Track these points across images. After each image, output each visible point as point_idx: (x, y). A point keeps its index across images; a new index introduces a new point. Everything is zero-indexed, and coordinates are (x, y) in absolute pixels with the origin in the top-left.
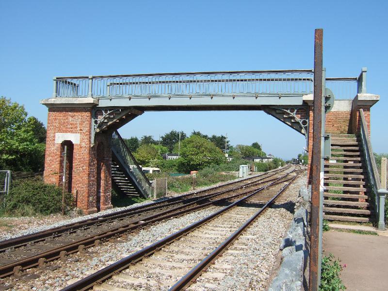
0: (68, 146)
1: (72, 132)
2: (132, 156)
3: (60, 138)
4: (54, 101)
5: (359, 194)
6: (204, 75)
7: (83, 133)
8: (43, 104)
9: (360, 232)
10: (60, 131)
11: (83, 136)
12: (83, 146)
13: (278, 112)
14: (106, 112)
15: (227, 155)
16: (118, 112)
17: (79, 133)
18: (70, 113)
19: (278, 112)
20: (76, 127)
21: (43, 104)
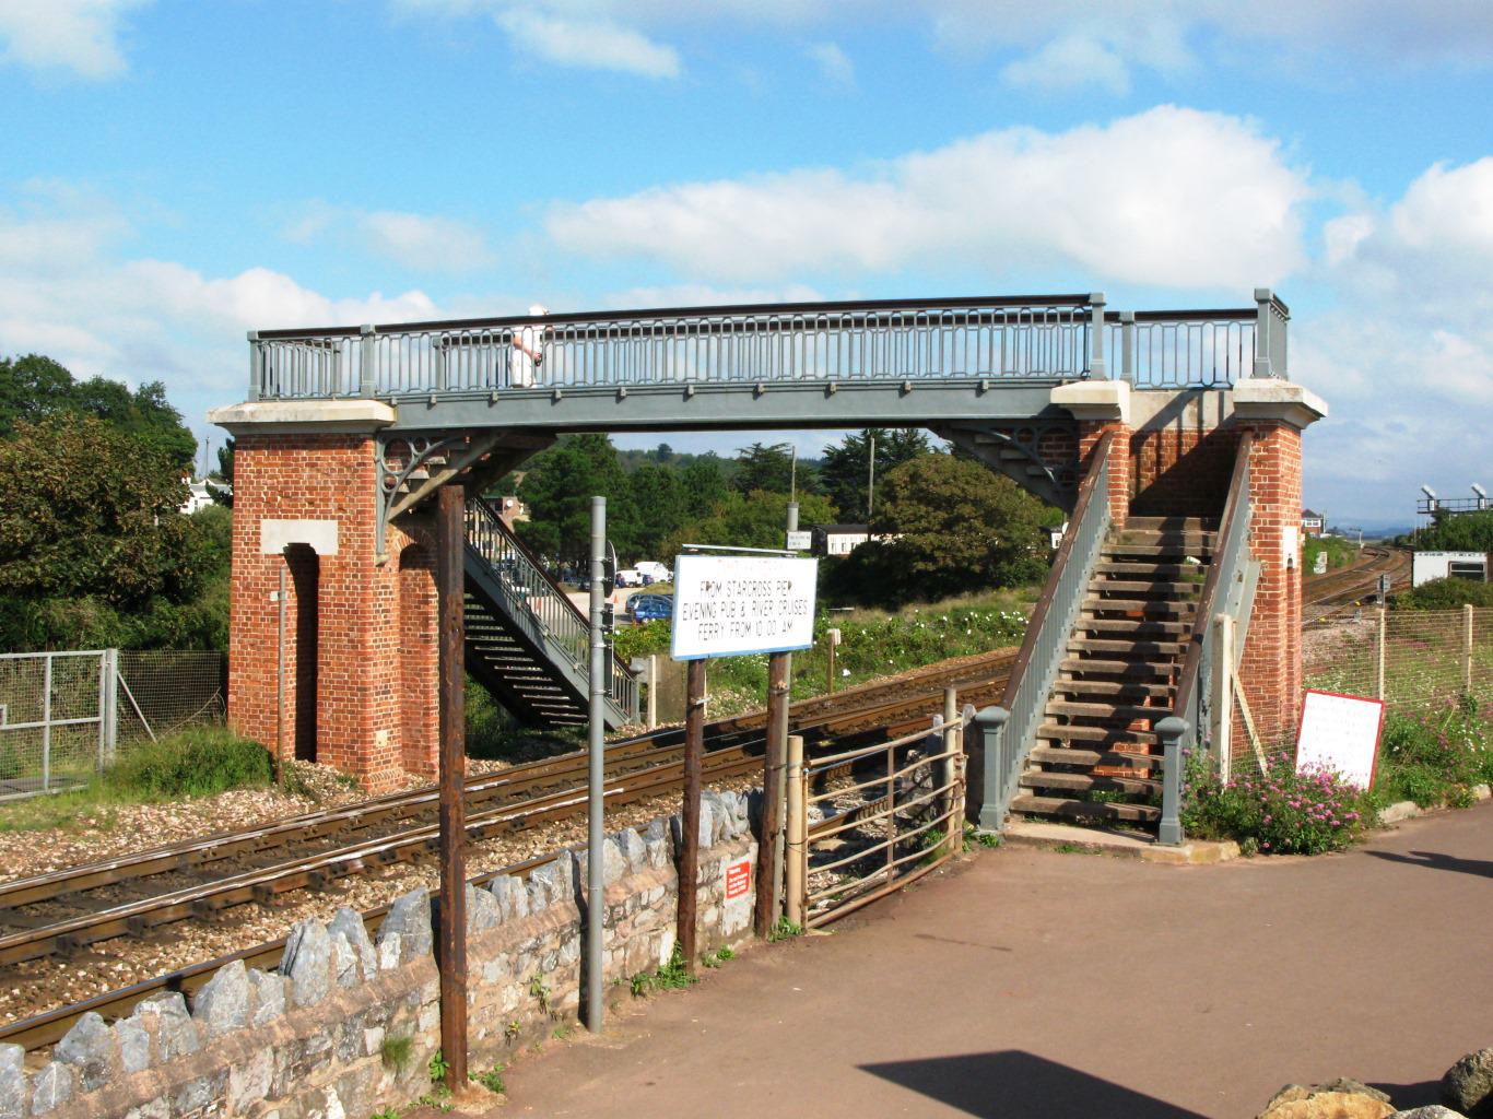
0: (302, 560)
1: (311, 515)
2: (592, 611)
3: (276, 535)
4: (252, 414)
5: (641, 710)
6: (830, 361)
7: (348, 518)
8: (217, 424)
9: (1066, 847)
10: (274, 512)
11: (348, 529)
12: (348, 564)
13: (979, 440)
14: (420, 448)
15: (923, 626)
16: (462, 447)
17: (333, 518)
18: (304, 453)
19: (979, 440)
20: (326, 500)
21: (217, 424)
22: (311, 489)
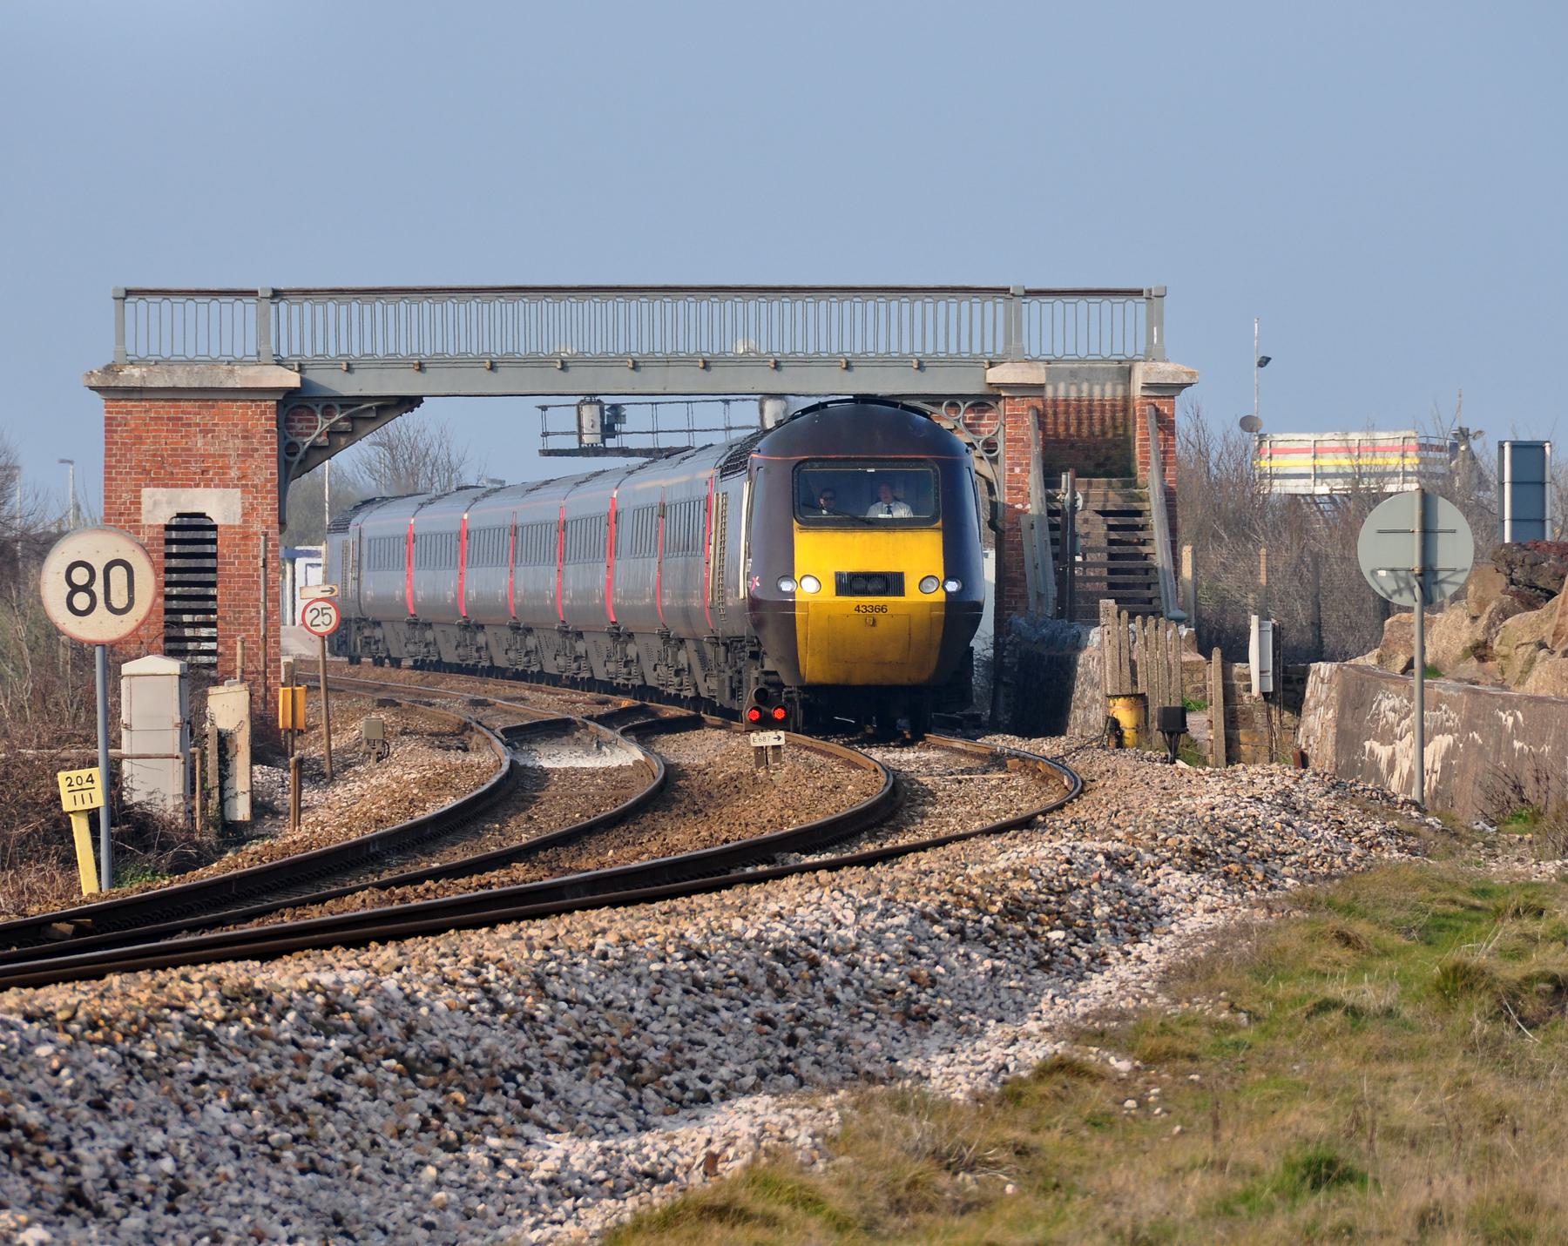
17: (236, 486)
22: (205, 457)
